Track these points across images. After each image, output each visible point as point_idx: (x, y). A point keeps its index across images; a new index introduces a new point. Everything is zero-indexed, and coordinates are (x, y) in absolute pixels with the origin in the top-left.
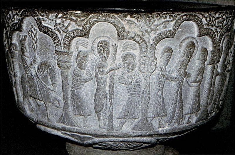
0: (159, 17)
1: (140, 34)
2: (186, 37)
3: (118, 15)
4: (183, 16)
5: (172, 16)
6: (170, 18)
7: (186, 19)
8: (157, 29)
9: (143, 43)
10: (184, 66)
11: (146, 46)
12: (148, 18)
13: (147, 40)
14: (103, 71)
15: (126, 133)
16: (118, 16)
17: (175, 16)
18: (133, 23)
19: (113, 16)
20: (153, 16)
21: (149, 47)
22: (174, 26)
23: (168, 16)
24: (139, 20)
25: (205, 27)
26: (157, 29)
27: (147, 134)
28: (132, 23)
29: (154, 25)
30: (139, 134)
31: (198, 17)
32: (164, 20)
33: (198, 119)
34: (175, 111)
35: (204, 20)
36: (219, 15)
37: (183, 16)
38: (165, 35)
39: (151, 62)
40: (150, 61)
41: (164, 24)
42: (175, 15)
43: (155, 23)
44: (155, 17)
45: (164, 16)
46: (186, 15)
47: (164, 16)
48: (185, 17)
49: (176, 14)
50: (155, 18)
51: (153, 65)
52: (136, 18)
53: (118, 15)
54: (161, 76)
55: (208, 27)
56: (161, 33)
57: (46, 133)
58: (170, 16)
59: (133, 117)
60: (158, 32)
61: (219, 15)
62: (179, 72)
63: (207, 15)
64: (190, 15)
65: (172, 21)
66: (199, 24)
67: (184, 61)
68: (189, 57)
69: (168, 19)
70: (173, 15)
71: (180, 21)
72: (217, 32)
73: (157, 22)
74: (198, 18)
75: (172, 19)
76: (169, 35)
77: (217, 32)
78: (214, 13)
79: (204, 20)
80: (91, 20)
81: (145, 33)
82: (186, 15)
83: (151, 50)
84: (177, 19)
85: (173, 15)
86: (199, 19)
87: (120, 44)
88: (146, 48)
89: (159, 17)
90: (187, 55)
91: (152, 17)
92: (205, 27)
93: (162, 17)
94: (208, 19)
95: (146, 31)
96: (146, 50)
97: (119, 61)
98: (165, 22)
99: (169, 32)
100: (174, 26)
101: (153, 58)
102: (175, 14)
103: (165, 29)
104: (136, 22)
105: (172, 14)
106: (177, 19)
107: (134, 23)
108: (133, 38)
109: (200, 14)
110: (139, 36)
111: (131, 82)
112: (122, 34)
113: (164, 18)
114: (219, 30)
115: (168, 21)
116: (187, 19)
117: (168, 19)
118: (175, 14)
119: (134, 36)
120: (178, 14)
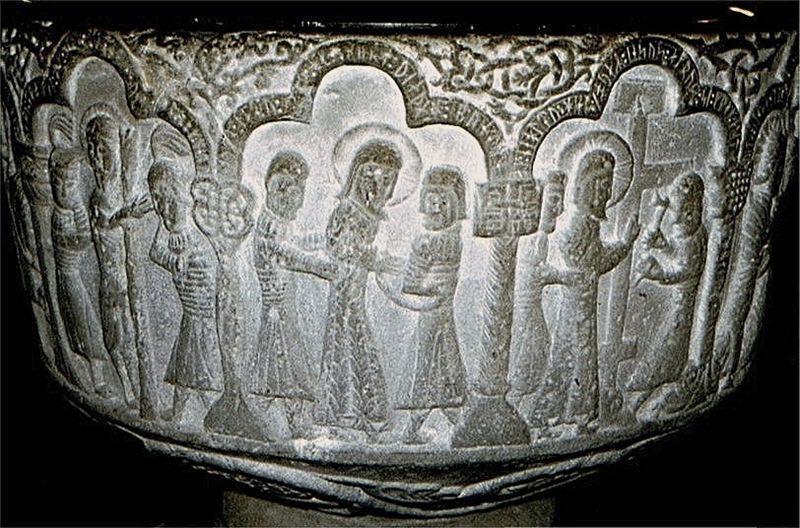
0: (242, 48)
1: (184, 99)
2: (364, 121)
3: (126, 37)
4: (327, 48)
5: (288, 46)
6: (278, 52)
7: (342, 58)
8: (238, 90)
9: (195, 133)
10: (352, 229)
11: (204, 145)
12: (206, 51)
13: (205, 126)
14: (101, 217)
15: (192, 435)
16: (125, 40)
17: (298, 45)
18: (163, 64)
19: (113, 37)
20: (223, 43)
21: (214, 147)
22: (295, 82)
23: (272, 46)
24: (179, 53)
25: (436, 91)
26: (238, 90)
27: (255, 450)
28: (160, 62)
29: (226, 75)
30: (231, 446)
31: (394, 53)
32: (260, 59)
33: (458, 434)
34: (343, 388)
35: (426, 68)
36: (514, 50)
37: (327, 48)
38: (264, 111)
39: (228, 202)
40: (224, 197)
41: (258, 71)
42: (301, 42)
43: (229, 68)
44: (229, 46)
45: (260, 45)
46: (341, 45)
47: (260, 45)
48: (334, 52)
49: (304, 40)
50: (229, 51)
51: (237, 211)
52: (170, 47)
53: (126, 37)
54: (269, 253)
55: (449, 95)
56: (251, 102)
57: (159, 453)
58: (279, 44)
59: (199, 383)
60: (241, 100)
61: (514, 50)
62: (335, 246)
63: (441, 47)
64: (362, 44)
65: (285, 62)
66: (403, 78)
67: (350, 208)
68: (368, 198)
69: (271, 55)
70: (293, 42)
71: (315, 66)
72: (506, 116)
73: (234, 66)
74: (396, 59)
75: (285, 56)
76: (280, 111)
77: (506, 116)
78: (487, 41)
79: (426, 68)
80: (64, 48)
81: (198, 98)
82: (341, 45)
83: (221, 159)
84: (305, 56)
85: (293, 42)
86: (400, 61)
87: (140, 133)
88: (207, 153)
89: (242, 48)
90: (358, 188)
91: (217, 45)
92: (436, 91)
93: (250, 47)
94: (447, 65)
95: (202, 94)
96: (206, 157)
97: (138, 191)
98: (262, 64)
99: (277, 102)
100: (295, 82)
101: (230, 190)
102: (300, 38)
103: (264, 92)
104: (172, 60)
105: (289, 40)
106: (305, 56)
107: (167, 62)
108: (163, 114)
109: (405, 43)
110: (181, 106)
111: (177, 263)
112: (137, 99)
113: (260, 54)
114: (511, 106)
115: (272, 62)
116: (345, 57)
117: (271, 55)
118: (300, 38)
119: (169, 106)
120: (311, 41)
